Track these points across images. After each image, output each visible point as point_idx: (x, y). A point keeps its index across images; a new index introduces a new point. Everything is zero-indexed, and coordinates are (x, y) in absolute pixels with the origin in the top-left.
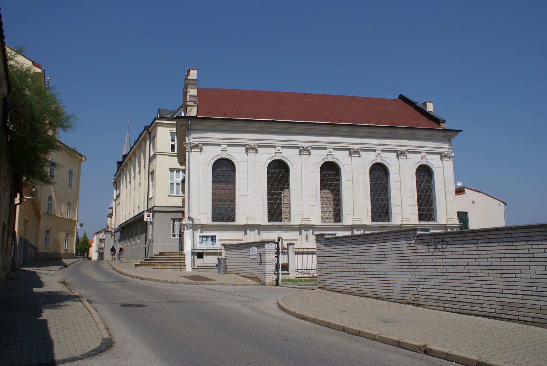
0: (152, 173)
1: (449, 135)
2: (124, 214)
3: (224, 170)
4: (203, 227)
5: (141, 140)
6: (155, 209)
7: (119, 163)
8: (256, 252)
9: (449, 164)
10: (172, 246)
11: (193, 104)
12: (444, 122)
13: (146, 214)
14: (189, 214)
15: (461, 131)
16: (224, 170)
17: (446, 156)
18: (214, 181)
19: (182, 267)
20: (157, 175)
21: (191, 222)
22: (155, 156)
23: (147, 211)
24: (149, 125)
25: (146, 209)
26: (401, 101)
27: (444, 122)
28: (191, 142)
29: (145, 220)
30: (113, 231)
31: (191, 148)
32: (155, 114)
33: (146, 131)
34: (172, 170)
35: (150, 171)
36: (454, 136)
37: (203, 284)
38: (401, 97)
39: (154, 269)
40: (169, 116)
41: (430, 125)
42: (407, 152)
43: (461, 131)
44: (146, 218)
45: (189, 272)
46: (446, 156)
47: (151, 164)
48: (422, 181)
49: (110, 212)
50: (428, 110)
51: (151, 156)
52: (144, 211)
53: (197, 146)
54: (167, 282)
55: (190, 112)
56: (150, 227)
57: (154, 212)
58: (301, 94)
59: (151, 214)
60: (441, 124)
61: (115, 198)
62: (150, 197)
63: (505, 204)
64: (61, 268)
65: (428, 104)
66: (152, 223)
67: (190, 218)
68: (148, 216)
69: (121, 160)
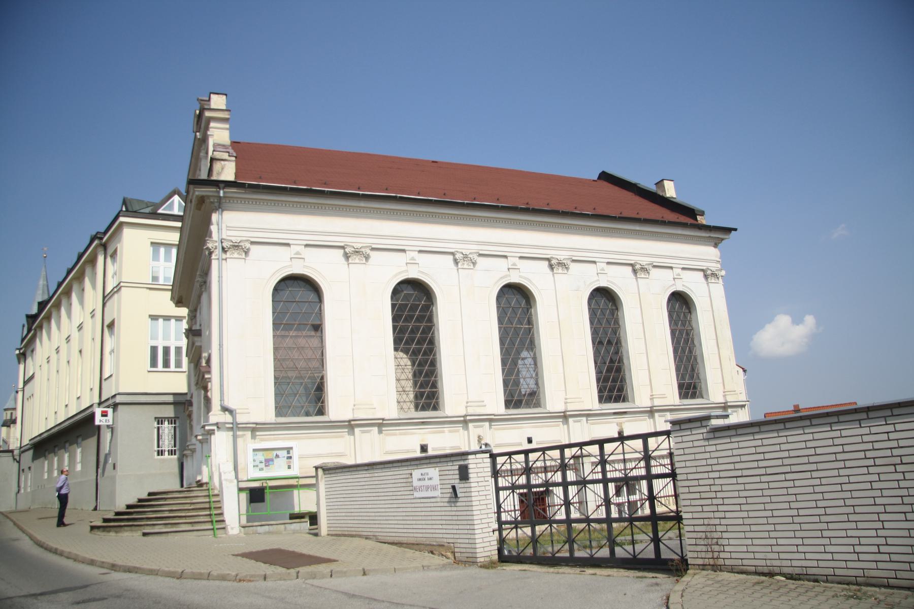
0: (111, 326)
1: (719, 233)
2: (43, 413)
3: (298, 297)
4: (255, 429)
5: (85, 262)
6: (118, 399)
7: (31, 318)
8: (436, 481)
9: (718, 289)
10: (161, 475)
11: (225, 156)
12: (702, 213)
13: (98, 411)
14: (222, 400)
15: (735, 230)
16: (298, 297)
17: (714, 275)
18: (276, 325)
19: (217, 526)
20: (123, 327)
21: (228, 418)
22: (118, 288)
23: (100, 404)
24: (103, 231)
25: (97, 400)
26: (605, 184)
27: (702, 213)
28: (224, 237)
29: (97, 423)
30: (16, 452)
31: (224, 250)
32: (118, 206)
33: (96, 242)
34: (154, 318)
35: (107, 322)
36: (722, 239)
37: (313, 576)
38: (605, 177)
39: (145, 534)
40: (147, 210)
41: (681, 218)
42: (650, 267)
43: (735, 230)
44: (99, 420)
45: (236, 538)
46: (714, 275)
47: (108, 305)
48: (676, 324)
49: (7, 416)
50: (668, 195)
51: (108, 290)
52: (91, 406)
53: (236, 247)
54: (209, 576)
55: (219, 174)
56: (106, 436)
57: (115, 406)
58: (427, 161)
59: (110, 411)
60: (699, 218)
61: (21, 385)
62: (106, 375)
63: (745, 371)
64: (59, 328)
65: (666, 183)
66: (111, 428)
67: (225, 409)
68: (104, 414)
69: (34, 310)
